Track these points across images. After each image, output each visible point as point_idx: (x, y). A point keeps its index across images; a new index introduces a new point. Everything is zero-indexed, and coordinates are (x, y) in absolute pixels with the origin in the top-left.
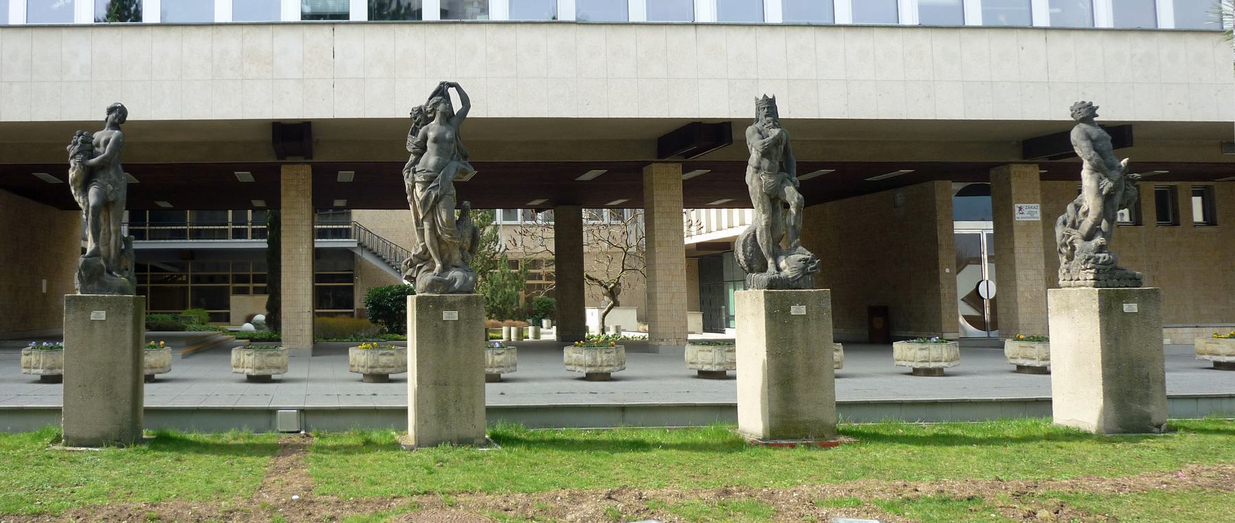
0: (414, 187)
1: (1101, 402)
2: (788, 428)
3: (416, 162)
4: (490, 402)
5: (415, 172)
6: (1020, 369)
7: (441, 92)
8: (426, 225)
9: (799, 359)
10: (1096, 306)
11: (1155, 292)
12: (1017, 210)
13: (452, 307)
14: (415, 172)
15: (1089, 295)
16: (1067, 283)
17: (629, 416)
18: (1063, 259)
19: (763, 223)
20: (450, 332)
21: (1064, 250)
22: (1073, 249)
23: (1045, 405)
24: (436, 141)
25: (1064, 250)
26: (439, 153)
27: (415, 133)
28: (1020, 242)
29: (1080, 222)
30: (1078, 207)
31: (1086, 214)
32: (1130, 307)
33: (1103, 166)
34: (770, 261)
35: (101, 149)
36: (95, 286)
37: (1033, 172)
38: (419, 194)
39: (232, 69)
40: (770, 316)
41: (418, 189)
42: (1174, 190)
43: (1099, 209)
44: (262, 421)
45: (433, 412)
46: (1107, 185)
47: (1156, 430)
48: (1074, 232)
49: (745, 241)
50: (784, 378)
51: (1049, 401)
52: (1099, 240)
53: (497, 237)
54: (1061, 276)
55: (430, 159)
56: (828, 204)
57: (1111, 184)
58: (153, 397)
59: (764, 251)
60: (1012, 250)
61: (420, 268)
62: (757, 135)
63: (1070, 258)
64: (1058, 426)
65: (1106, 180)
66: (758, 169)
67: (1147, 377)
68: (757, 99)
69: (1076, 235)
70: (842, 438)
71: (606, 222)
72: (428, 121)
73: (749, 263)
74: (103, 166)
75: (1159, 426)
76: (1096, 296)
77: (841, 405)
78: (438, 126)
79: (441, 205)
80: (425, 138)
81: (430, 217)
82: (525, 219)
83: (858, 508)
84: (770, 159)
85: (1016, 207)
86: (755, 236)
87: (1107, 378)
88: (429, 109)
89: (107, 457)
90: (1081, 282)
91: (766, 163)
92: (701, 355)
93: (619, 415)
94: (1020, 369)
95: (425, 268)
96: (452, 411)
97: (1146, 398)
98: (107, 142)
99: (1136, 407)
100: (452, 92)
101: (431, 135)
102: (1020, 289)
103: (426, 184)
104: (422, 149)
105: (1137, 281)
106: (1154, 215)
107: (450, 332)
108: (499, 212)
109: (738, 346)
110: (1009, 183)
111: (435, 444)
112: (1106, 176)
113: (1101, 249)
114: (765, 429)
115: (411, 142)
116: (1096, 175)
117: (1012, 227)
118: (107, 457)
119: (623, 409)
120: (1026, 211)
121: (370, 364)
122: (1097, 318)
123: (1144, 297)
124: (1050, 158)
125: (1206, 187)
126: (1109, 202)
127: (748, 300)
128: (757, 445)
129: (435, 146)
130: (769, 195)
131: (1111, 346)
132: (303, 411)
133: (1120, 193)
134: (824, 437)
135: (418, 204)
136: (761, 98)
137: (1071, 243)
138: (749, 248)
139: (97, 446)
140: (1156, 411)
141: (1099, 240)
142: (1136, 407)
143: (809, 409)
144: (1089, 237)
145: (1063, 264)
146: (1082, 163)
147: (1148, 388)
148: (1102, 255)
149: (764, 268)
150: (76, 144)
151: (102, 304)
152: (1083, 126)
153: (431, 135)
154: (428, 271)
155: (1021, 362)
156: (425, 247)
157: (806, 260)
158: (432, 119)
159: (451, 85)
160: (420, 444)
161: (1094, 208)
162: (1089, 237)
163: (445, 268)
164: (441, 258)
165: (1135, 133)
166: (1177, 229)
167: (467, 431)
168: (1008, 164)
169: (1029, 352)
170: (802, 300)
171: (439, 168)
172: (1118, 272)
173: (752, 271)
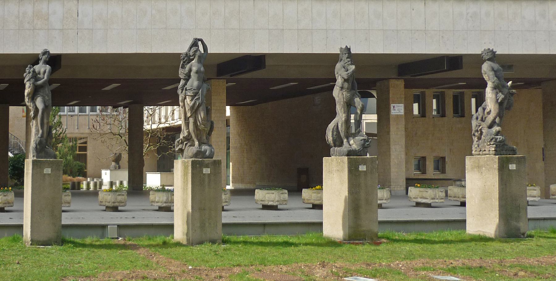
0: (185, 98)
1: (497, 220)
2: (357, 235)
3: (186, 84)
4: (224, 221)
5: (186, 90)
6: (418, 204)
7: (194, 44)
8: (191, 120)
9: (363, 195)
10: (496, 166)
11: (524, 157)
12: (392, 107)
13: (207, 166)
14: (186, 90)
15: (493, 160)
16: (477, 153)
17: (267, 229)
18: (475, 139)
19: (343, 119)
20: (207, 180)
21: (476, 134)
22: (481, 133)
23: (462, 223)
24: (197, 72)
25: (476, 134)
26: (199, 79)
27: (183, 67)
28: (393, 128)
29: (485, 118)
30: (484, 109)
31: (489, 113)
32: (513, 167)
33: (500, 86)
34: (345, 140)
35: (41, 76)
36: (43, 154)
37: (401, 83)
38: (189, 102)
39: (28, 23)
40: (350, 171)
41: (188, 100)
42: (423, 94)
43: (497, 111)
44: (100, 232)
45: (198, 225)
46: (501, 96)
47: (522, 236)
48: (482, 123)
49: (333, 129)
50: (357, 206)
51: (465, 221)
52: (496, 128)
53: (61, 123)
54: (474, 149)
55: (194, 82)
56: (270, 103)
57: (503, 96)
58: (66, 219)
59: (342, 134)
60: (388, 133)
61: (186, 144)
62: (343, 69)
63: (479, 138)
64: (469, 235)
65: (500, 94)
66: (342, 88)
67: (519, 206)
68: (341, 48)
69: (484, 125)
70: (383, 240)
71: (66, 113)
72: (190, 60)
73: (334, 141)
74: (42, 86)
75: (523, 234)
76: (497, 160)
77: (381, 223)
78: (196, 64)
79: (201, 108)
80: (190, 70)
81: (194, 115)
82: (101, 111)
83: (452, 271)
84: (348, 82)
85: (392, 105)
86: (337, 126)
87: (501, 206)
88: (191, 54)
89: (60, 250)
90: (487, 152)
91: (346, 85)
92: (267, 196)
93: (260, 229)
94: (418, 204)
95: (189, 144)
96: (207, 224)
97: (518, 219)
98: (45, 72)
99: (514, 223)
100: (200, 43)
101: (194, 69)
102: (393, 157)
103: (193, 97)
104: (188, 77)
105: (514, 152)
106: (452, 111)
107: (207, 180)
108: (88, 108)
109: (175, 193)
110: (388, 92)
111: (201, 243)
112: (500, 91)
113: (498, 133)
114: (344, 235)
115: (182, 73)
116: (495, 91)
117: (389, 119)
118: (60, 250)
119: (264, 225)
120: (396, 108)
121: (113, 201)
122: (497, 173)
123: (519, 161)
124: (411, 76)
125: (478, 92)
126: (504, 107)
127: (334, 163)
128: (388, 238)
129: (197, 75)
130: (347, 103)
131: (503, 188)
132: (119, 226)
133: (506, 101)
134: (375, 240)
135: (187, 108)
136: (344, 47)
137: (481, 130)
138: (335, 133)
139: (50, 245)
140: (523, 226)
141: (496, 128)
142: (514, 223)
143: (367, 225)
144: (490, 127)
145: (475, 142)
146: (487, 84)
147: (519, 213)
148: (499, 137)
149: (341, 144)
150: (29, 73)
151: (50, 164)
152: (489, 62)
153: (194, 69)
154: (190, 146)
155: (420, 200)
156: (189, 133)
157: (364, 140)
158: (193, 60)
159: (199, 40)
160: (191, 242)
161: (495, 110)
162: (490, 127)
163: (200, 145)
164: (199, 141)
165: (464, 60)
166: (463, 119)
167: (214, 236)
168: (388, 79)
169: (425, 194)
170: (364, 162)
171: (199, 88)
172: (506, 147)
173: (335, 146)
